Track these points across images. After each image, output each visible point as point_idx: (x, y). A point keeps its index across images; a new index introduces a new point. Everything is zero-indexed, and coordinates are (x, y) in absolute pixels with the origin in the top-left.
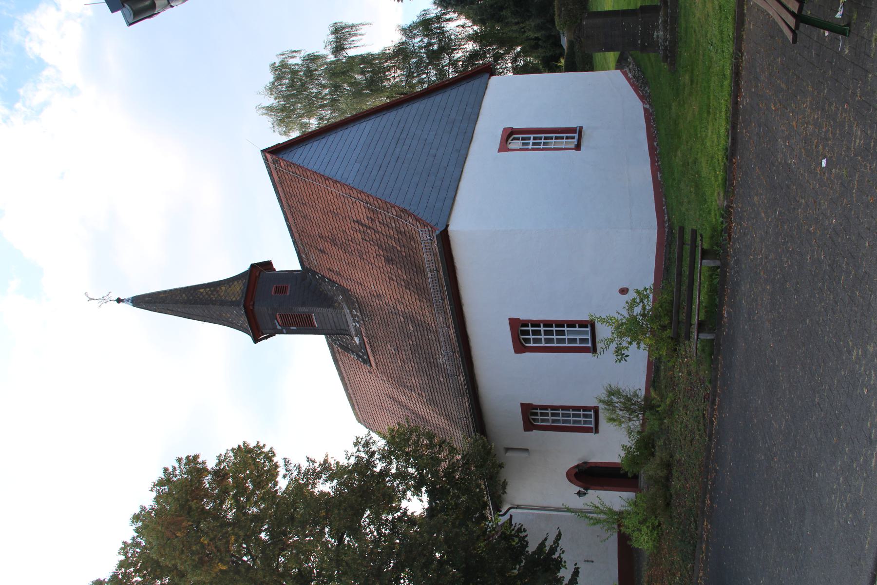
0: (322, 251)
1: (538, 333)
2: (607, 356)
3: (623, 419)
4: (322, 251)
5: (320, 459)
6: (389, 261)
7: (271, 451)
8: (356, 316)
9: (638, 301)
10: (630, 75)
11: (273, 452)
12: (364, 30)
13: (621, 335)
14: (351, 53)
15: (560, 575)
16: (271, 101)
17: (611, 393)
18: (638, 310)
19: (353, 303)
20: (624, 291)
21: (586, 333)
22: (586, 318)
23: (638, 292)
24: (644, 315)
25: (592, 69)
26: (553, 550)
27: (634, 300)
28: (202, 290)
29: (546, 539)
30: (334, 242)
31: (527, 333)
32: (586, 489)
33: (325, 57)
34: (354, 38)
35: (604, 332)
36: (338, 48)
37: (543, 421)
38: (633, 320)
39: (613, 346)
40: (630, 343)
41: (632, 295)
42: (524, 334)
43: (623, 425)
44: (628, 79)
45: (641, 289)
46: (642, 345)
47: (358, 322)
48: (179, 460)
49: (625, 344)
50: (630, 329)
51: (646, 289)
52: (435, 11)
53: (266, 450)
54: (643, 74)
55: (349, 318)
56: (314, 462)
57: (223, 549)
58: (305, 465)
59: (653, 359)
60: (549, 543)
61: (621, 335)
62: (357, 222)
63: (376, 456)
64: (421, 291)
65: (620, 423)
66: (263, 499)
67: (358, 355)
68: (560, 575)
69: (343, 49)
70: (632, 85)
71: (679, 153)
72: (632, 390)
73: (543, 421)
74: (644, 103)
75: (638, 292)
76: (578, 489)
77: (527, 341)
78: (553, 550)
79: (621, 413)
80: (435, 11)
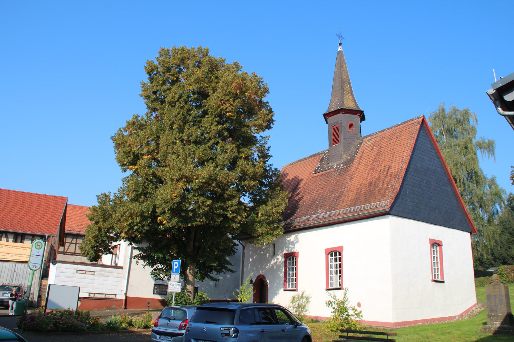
0: (372, 148)
1: (336, 261)
2: (327, 296)
3: (294, 304)
4: (372, 148)
5: (270, 153)
6: (370, 184)
7: (271, 128)
8: (340, 167)
9: (356, 312)
10: (474, 308)
11: (270, 128)
12: (492, 158)
13: (339, 305)
14: (478, 152)
15: (213, 271)
16: (448, 110)
17: (307, 298)
18: (351, 312)
19: (346, 165)
20: (359, 305)
21: (336, 285)
22: (345, 286)
23: (361, 312)
24: (348, 315)
25: (476, 286)
26: (226, 269)
27: (356, 310)
28: (348, 86)
29: (231, 265)
30: (378, 154)
31: (336, 255)
32: (254, 285)
33: (474, 138)
34: (487, 153)
35: (339, 295)
36: (480, 146)
37: (289, 263)
38: (346, 309)
39: (332, 300)
40: (334, 308)
41: (359, 309)
42: (335, 254)
43: (291, 304)
44: (472, 308)
45: (362, 314)
46: (333, 314)
47: (336, 167)
48: (267, 85)
49: (334, 305)
50: (342, 309)
51: (362, 317)
52: (505, 197)
53: (271, 125)
54: (475, 316)
55: (339, 162)
56: (268, 150)
57: (228, 110)
58: (267, 146)
59: (279, 313)
60: (229, 267)
61: (339, 305)
62: (390, 167)
63: (270, 179)
64: (355, 202)
65: (292, 303)
66: (176, 77)
67: (318, 167)
68: (213, 271)
69: (480, 148)
70: (469, 310)
71: (433, 334)
72: (309, 309)
73: (289, 263)
74: (459, 316)
75: (361, 312)
76: (254, 280)
77: (332, 255)
78: (226, 269)
79: (297, 303)
80: (505, 197)
